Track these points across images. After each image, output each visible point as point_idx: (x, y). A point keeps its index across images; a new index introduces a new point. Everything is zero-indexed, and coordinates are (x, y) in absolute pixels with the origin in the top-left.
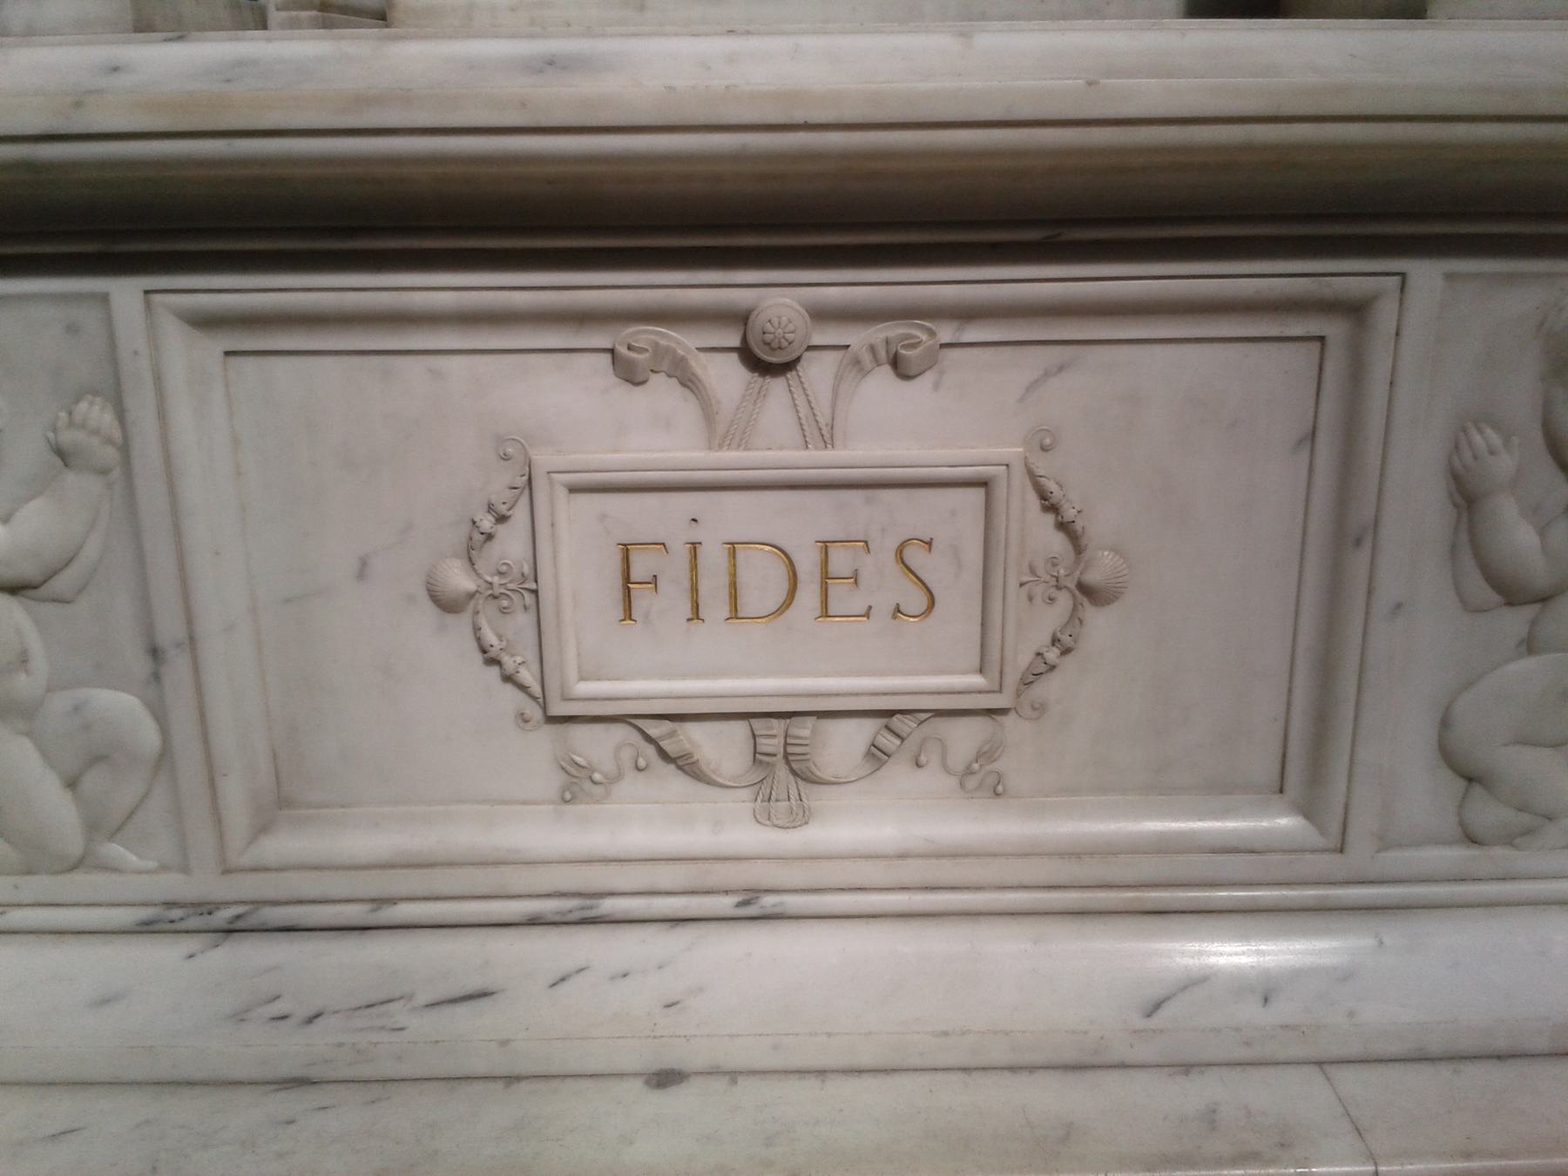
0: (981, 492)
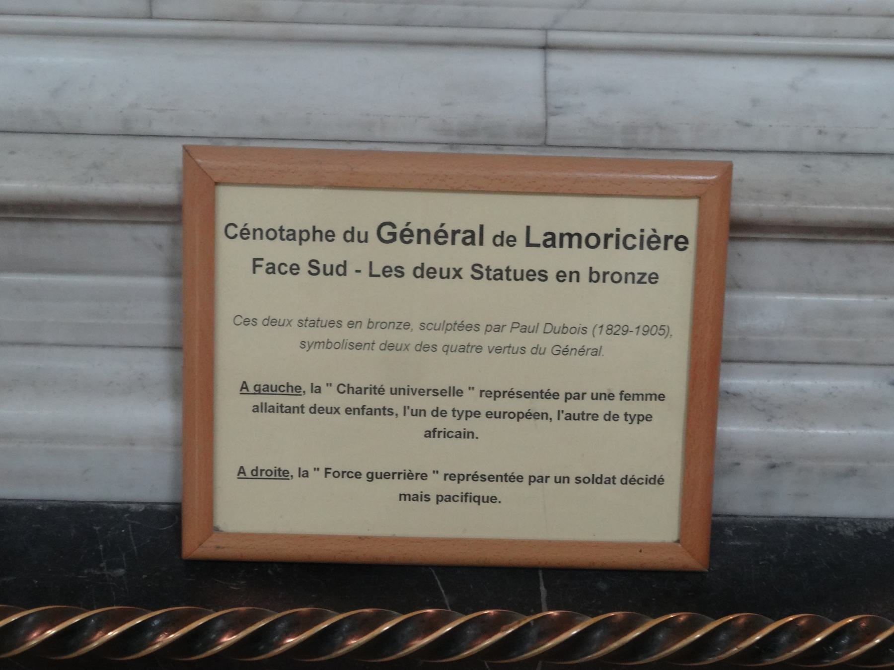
0: (531, 242)
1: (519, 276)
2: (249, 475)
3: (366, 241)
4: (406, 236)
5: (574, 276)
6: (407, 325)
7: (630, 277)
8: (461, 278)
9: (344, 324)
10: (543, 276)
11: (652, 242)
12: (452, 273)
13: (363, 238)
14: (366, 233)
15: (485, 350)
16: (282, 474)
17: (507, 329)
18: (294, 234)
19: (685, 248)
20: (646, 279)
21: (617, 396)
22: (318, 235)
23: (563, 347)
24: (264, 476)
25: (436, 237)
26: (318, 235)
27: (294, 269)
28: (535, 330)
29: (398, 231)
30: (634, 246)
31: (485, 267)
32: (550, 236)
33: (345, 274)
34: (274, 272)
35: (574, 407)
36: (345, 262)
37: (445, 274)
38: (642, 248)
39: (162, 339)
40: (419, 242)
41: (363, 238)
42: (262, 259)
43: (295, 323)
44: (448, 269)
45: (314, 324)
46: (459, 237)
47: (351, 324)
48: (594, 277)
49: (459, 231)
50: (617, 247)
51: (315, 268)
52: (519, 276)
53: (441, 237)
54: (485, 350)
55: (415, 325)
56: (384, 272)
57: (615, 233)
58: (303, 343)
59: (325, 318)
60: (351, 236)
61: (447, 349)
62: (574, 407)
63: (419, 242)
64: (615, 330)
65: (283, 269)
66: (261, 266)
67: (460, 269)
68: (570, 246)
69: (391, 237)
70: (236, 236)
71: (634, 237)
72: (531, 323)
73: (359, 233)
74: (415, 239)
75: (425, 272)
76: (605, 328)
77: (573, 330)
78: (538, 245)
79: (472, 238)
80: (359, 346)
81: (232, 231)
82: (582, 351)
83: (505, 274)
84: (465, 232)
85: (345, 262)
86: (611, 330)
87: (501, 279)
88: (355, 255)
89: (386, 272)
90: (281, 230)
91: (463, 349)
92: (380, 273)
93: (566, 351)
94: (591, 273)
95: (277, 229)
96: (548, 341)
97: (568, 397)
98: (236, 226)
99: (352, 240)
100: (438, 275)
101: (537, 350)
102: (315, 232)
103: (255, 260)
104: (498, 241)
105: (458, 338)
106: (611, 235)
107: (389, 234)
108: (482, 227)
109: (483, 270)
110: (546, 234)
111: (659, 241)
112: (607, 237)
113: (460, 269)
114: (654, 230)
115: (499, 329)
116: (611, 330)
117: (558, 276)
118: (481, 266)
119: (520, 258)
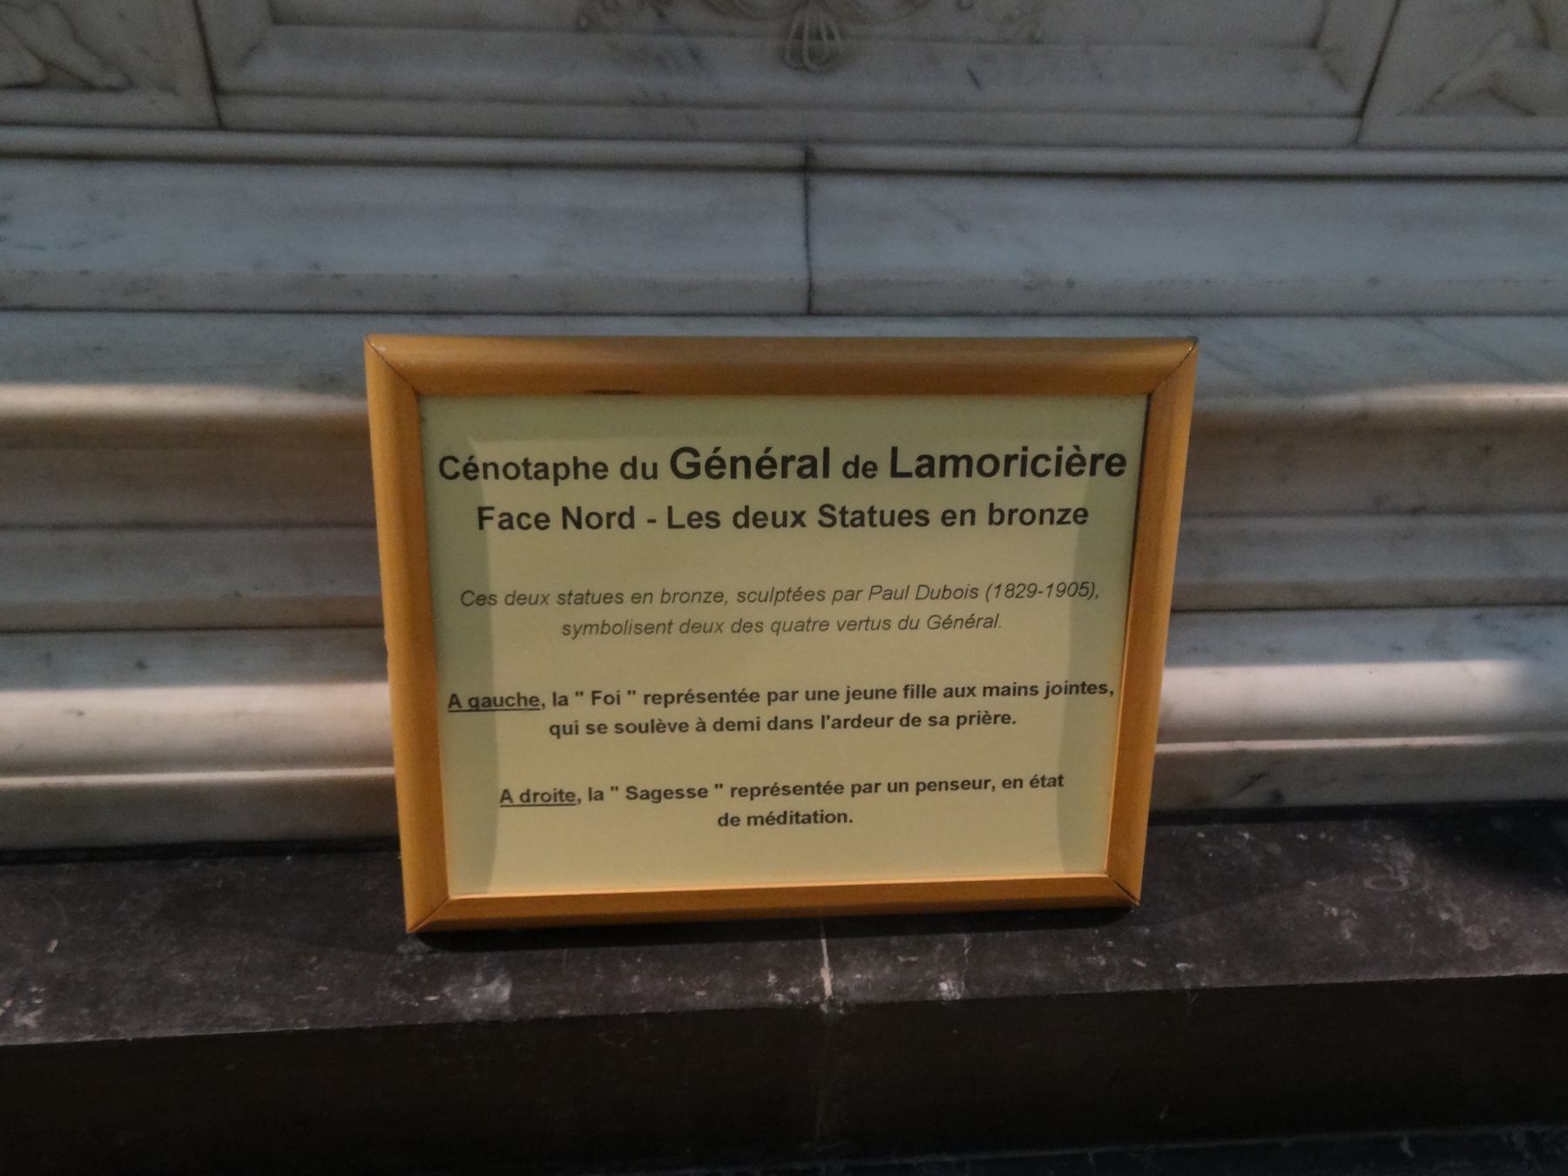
0: (899, 470)
1: (887, 519)
2: (517, 801)
3: (655, 476)
4: (715, 467)
5: (968, 516)
6: (719, 597)
7: (1047, 515)
8: (803, 525)
9: (627, 598)
10: (922, 518)
11: (1072, 465)
12: (791, 519)
13: (649, 472)
14: (655, 465)
15: (833, 627)
16: (564, 798)
17: (865, 595)
18: (546, 470)
19: (1120, 472)
20: (1070, 517)
21: (901, 693)
22: (581, 470)
23: (944, 617)
24: (539, 801)
25: (759, 467)
26: (581, 470)
27: (542, 521)
28: (904, 595)
29: (702, 460)
30: (1047, 472)
31: (838, 509)
32: (925, 461)
33: (632, 525)
34: (511, 527)
35: (784, 710)
36: (632, 508)
37: (779, 520)
38: (1058, 473)
39: (499, 614)
40: (734, 475)
41: (649, 472)
42: (492, 508)
43: (553, 599)
44: (785, 514)
45: (581, 599)
46: (793, 467)
47: (636, 598)
48: (997, 517)
49: (792, 458)
50: (1023, 473)
51: (574, 518)
52: (887, 519)
53: (765, 467)
54: (833, 627)
55: (731, 596)
56: (690, 520)
57: (1021, 453)
58: (566, 627)
59: (599, 589)
60: (632, 470)
61: (778, 627)
62: (784, 710)
63: (734, 475)
64: (1017, 591)
65: (525, 521)
66: (491, 518)
67: (803, 513)
68: (956, 474)
69: (691, 470)
70: (457, 475)
71: (1047, 458)
72: (898, 586)
73: (644, 465)
74: (728, 471)
75: (749, 519)
76: (1003, 589)
77: (958, 594)
78: (909, 475)
79: (811, 467)
80: (649, 629)
81: (450, 468)
82: (971, 622)
83: (867, 517)
84: (801, 459)
85: (632, 508)
86: (1012, 591)
87: (862, 524)
88: (649, 497)
89: (694, 520)
90: (526, 463)
91: (802, 626)
92: (685, 522)
93: (947, 623)
94: (992, 511)
95: (519, 462)
96: (924, 610)
97: (772, 697)
98: (456, 460)
99: (634, 476)
100: (770, 522)
101: (908, 624)
102: (576, 466)
103: (481, 509)
104: (851, 470)
105: (792, 611)
106: (1016, 457)
107: (689, 465)
108: (826, 451)
109: (836, 514)
110: (920, 458)
111: (1083, 463)
112: (1009, 459)
113: (803, 513)
114: (1077, 447)
115: (852, 596)
116: (1012, 591)
117: (944, 518)
118: (833, 508)
119: (884, 493)
